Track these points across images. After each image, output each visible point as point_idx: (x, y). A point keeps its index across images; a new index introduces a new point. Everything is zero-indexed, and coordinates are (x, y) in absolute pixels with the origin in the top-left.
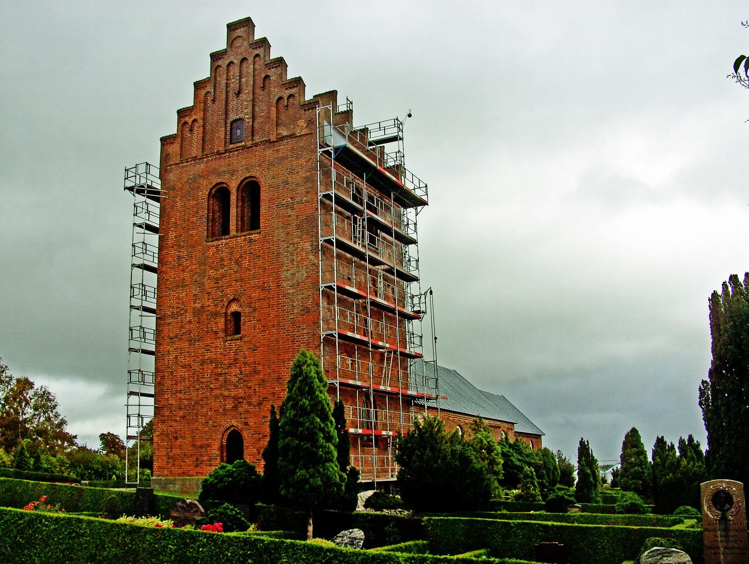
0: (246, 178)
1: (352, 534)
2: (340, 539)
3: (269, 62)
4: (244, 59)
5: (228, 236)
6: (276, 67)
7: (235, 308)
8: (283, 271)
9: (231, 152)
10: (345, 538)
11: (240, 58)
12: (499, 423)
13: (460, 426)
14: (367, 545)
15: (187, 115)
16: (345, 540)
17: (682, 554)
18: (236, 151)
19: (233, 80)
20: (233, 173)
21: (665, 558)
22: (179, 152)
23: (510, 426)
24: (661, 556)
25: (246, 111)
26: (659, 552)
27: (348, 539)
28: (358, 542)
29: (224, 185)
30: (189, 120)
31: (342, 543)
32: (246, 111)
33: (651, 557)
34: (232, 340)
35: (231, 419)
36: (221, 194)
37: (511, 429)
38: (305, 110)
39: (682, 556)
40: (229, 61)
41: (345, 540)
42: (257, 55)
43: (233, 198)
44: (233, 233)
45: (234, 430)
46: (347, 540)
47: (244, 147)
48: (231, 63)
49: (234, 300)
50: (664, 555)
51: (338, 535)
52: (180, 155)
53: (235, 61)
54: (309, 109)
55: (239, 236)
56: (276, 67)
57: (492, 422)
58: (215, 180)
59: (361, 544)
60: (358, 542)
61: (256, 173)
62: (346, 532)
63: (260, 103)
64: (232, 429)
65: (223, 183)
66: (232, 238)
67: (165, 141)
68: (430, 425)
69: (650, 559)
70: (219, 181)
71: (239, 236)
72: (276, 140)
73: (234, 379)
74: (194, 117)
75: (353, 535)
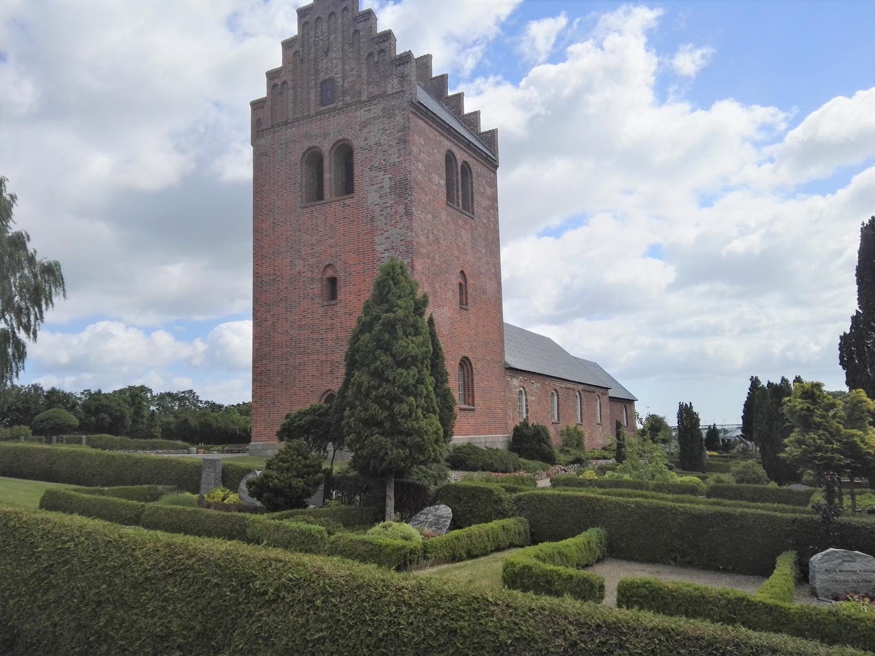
0: (338, 141)
1: (438, 511)
2: (424, 517)
3: (358, 15)
4: (332, 14)
5: (321, 202)
6: (365, 20)
7: (330, 273)
8: (377, 235)
9: (322, 114)
10: (430, 516)
11: (328, 12)
12: (594, 388)
13: (555, 390)
14: (456, 524)
15: (276, 77)
16: (429, 518)
17: (870, 559)
18: (328, 113)
19: (321, 38)
20: (326, 135)
21: (846, 564)
22: (269, 116)
23: (604, 391)
24: (840, 561)
25: (335, 70)
26: (838, 555)
27: (433, 517)
28: (445, 521)
29: (317, 149)
30: (278, 82)
31: (427, 522)
32: (335, 70)
33: (826, 561)
34: (328, 305)
35: (826, 397)
36: (314, 159)
37: (606, 394)
38: (396, 66)
39: (869, 561)
40: (316, 17)
41: (429, 518)
42: (346, 9)
43: (326, 163)
44: (327, 196)
45: (331, 394)
46: (431, 518)
47: (334, 109)
48: (319, 18)
49: (329, 265)
50: (845, 559)
51: (422, 512)
52: (272, 119)
53: (322, 16)
54: (399, 65)
55: (332, 201)
56: (365, 20)
57: (586, 387)
58: (307, 144)
59: (448, 523)
60: (445, 521)
61: (348, 135)
62: (432, 508)
63: (350, 61)
64: (329, 393)
65: (315, 147)
66: (327, 203)
67: (256, 106)
68: (807, 432)
69: (825, 564)
70: (311, 145)
71: (332, 201)
72: (367, 99)
73: (330, 343)
74: (283, 79)
75: (439, 513)
